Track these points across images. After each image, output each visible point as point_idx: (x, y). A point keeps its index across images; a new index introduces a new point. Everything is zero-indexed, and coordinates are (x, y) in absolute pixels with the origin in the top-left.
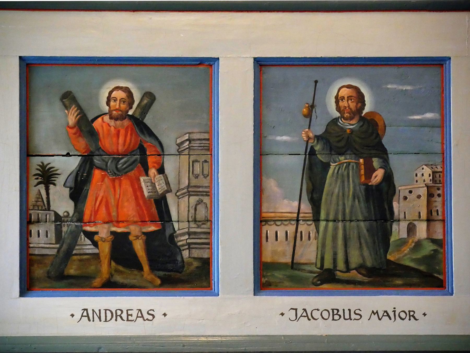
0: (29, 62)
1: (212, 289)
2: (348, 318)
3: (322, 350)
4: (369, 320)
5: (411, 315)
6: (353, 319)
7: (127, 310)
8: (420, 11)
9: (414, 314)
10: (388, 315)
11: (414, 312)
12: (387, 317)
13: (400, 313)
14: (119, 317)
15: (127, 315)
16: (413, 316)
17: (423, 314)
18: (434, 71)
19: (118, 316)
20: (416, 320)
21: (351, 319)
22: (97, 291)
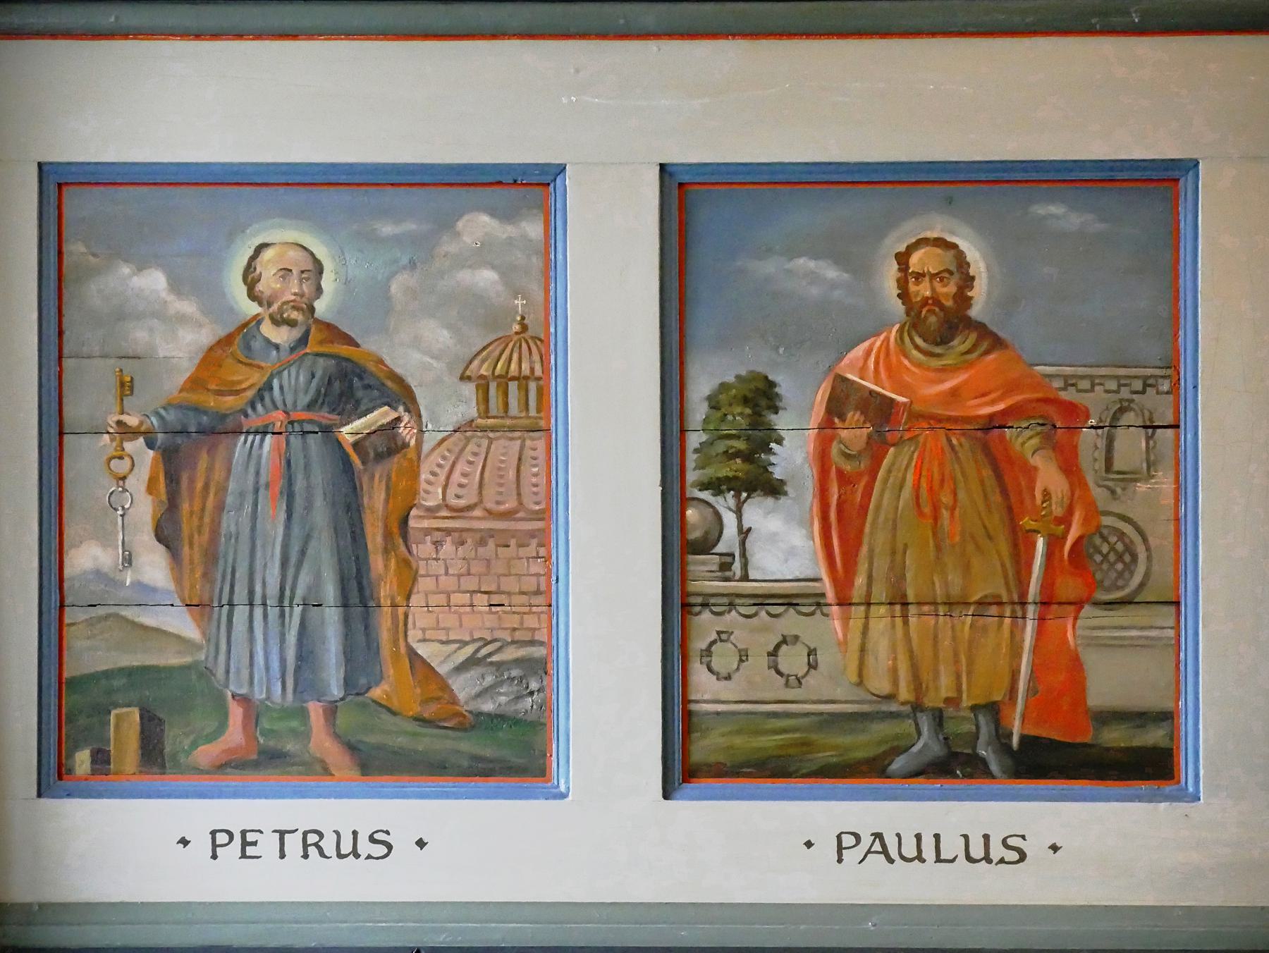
0: (686, 178)
1: (1179, 782)
2: (982, 855)
3: (1116, 948)
4: (860, 863)
5: (312, 843)
6: (995, 861)
7: (244, 833)
8: (914, 38)
9: (320, 841)
10: (885, 851)
11: (321, 835)
12: (882, 856)
13: (855, 843)
14: (312, 851)
15: (242, 844)
16: (316, 845)
17: (809, 848)
18: (79, 205)
19: (310, 845)
20: (321, 856)
21: (357, 856)
22: (206, 783)
